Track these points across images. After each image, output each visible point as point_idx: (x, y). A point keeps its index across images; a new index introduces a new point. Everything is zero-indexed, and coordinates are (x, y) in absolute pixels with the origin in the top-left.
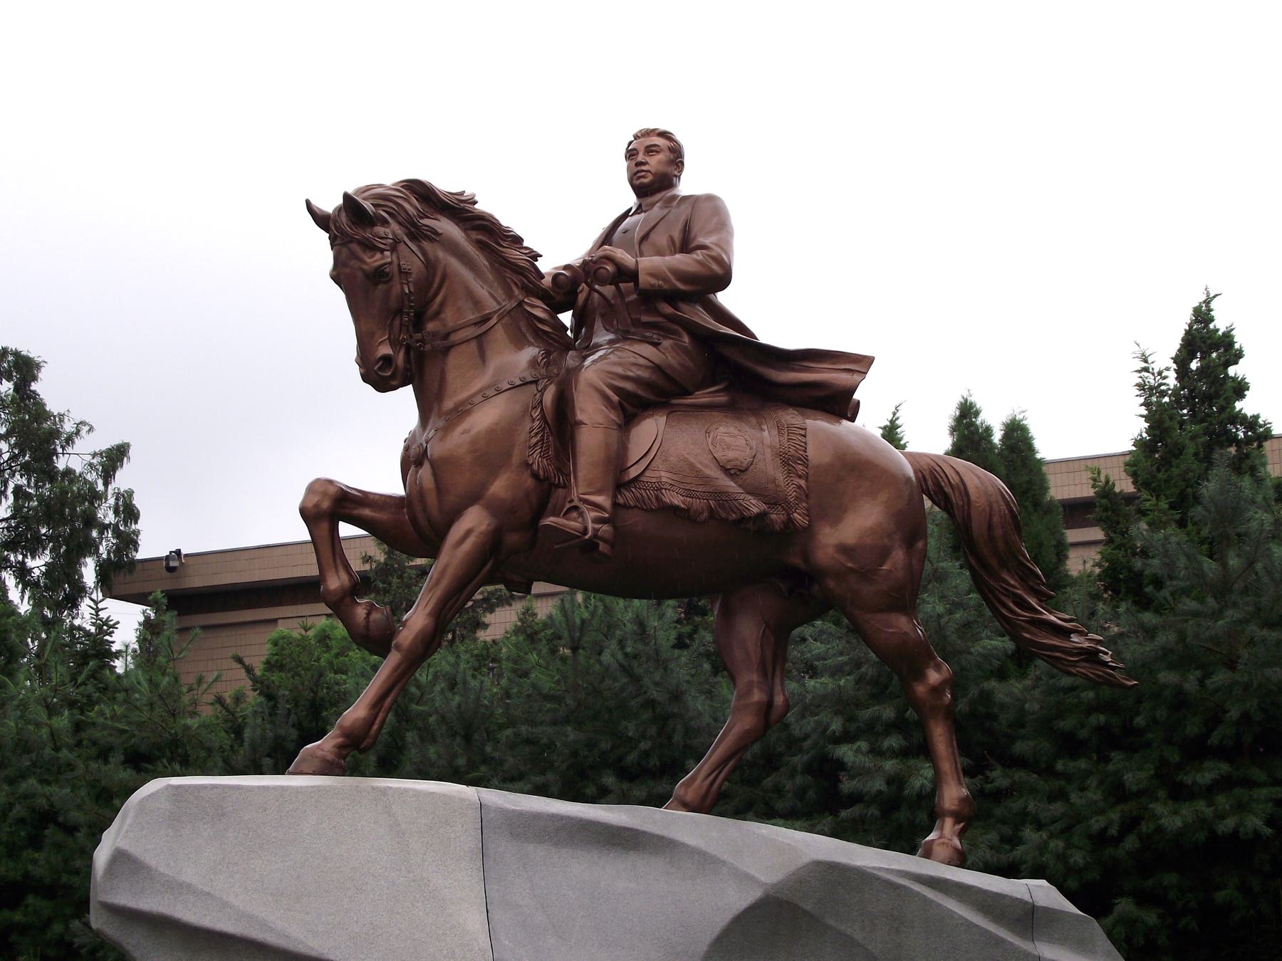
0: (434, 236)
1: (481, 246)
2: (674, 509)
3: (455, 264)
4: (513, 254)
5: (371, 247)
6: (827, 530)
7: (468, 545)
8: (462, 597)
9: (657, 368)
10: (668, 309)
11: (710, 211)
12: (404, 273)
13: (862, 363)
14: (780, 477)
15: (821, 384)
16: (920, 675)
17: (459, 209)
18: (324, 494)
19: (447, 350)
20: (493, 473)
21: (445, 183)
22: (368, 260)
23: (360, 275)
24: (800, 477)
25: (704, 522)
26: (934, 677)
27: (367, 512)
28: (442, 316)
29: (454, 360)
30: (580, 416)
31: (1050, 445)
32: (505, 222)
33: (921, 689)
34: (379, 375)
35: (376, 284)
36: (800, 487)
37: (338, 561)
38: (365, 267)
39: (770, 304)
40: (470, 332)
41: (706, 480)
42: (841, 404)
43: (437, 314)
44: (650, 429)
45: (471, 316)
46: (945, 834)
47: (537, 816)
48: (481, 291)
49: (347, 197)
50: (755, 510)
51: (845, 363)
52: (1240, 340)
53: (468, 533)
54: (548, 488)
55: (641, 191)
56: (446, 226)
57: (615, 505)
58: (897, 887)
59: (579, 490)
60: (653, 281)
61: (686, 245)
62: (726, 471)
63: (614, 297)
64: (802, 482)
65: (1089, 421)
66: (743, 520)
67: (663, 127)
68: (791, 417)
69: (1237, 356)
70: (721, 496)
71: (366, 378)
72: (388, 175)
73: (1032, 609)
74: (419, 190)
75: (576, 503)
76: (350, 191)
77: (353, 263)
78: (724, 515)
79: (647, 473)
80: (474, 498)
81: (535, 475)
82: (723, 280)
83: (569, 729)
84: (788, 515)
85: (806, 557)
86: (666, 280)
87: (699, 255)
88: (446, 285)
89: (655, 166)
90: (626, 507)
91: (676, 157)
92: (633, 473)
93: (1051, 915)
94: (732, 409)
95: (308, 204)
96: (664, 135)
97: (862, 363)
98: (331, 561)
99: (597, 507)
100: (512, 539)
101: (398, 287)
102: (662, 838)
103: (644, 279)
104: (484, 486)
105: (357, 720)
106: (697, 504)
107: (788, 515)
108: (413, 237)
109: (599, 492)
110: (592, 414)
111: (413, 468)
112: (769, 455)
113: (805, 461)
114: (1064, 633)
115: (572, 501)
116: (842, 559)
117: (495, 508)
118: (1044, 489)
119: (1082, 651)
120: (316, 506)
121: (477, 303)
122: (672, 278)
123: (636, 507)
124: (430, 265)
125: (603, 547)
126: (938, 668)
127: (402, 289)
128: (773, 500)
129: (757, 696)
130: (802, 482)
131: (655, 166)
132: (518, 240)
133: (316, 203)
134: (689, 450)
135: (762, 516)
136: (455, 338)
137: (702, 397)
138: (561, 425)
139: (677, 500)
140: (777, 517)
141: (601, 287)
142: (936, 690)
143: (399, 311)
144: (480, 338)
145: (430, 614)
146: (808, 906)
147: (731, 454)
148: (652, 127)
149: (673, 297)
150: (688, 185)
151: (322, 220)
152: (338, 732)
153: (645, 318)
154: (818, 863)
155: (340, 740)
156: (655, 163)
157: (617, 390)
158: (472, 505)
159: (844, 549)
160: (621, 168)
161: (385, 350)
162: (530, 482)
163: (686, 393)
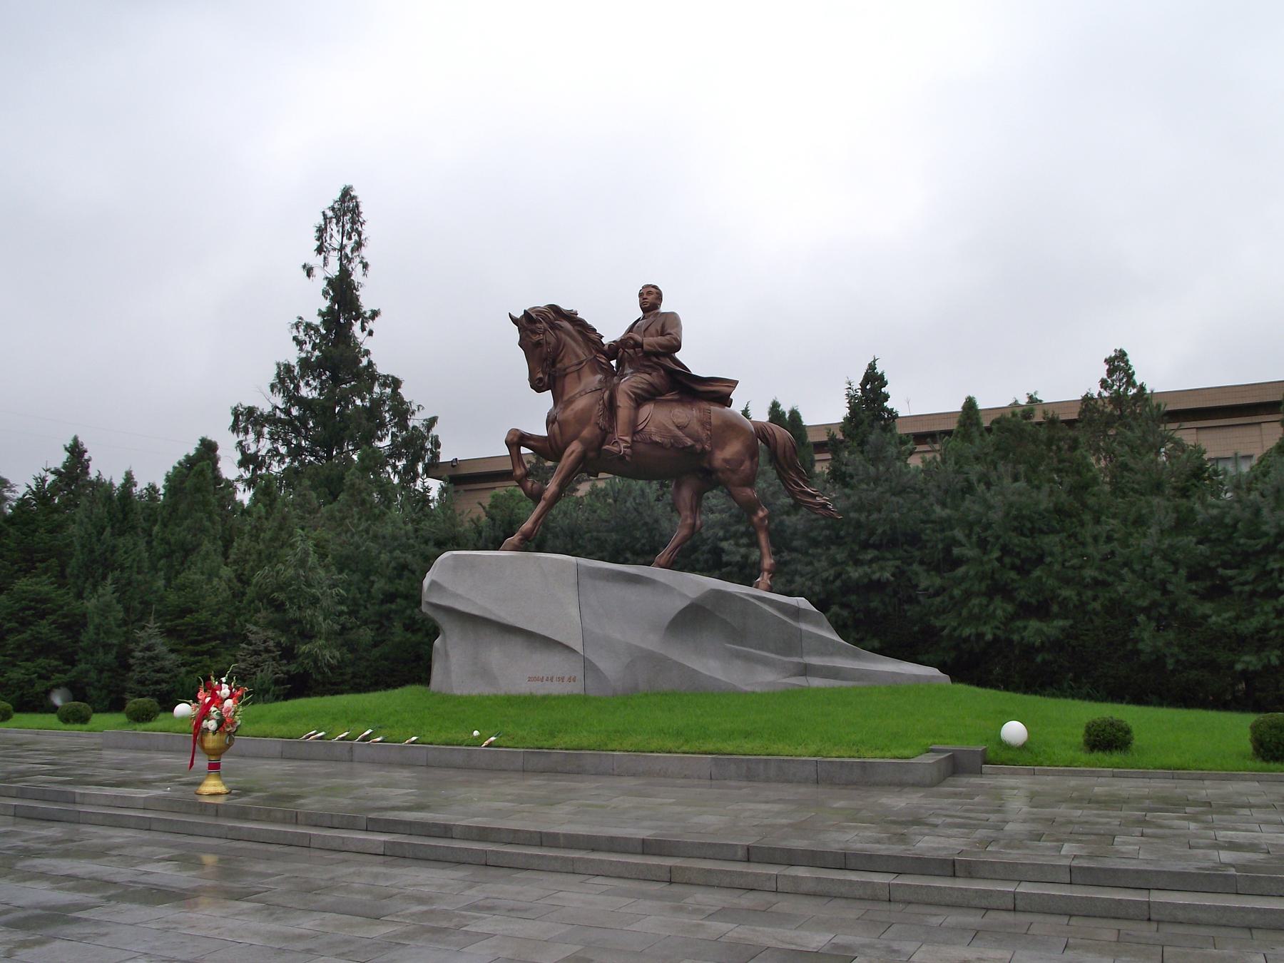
0: (561, 328)
1: (579, 332)
7: (573, 457)
9: (651, 384)
11: (673, 319)
16: (755, 513)
17: (571, 317)
21: (565, 306)
26: (761, 514)
34: (538, 386)
39: (696, 358)
42: (725, 400)
44: (647, 410)
45: (575, 362)
47: (599, 569)
48: (580, 352)
54: (605, 434)
56: (566, 324)
57: (633, 441)
66: (685, 448)
69: (885, 384)
72: (542, 303)
74: (554, 309)
82: (678, 348)
87: (668, 337)
89: (650, 298)
91: (659, 296)
93: (806, 612)
94: (680, 401)
96: (655, 287)
113: (710, 424)
117: (583, 442)
121: (577, 356)
124: (558, 340)
131: (650, 298)
135: (692, 446)
139: (658, 439)
140: (698, 447)
142: (762, 519)
143: (546, 359)
149: (657, 355)
150: (664, 308)
151: (515, 321)
156: (650, 298)
162: (598, 431)
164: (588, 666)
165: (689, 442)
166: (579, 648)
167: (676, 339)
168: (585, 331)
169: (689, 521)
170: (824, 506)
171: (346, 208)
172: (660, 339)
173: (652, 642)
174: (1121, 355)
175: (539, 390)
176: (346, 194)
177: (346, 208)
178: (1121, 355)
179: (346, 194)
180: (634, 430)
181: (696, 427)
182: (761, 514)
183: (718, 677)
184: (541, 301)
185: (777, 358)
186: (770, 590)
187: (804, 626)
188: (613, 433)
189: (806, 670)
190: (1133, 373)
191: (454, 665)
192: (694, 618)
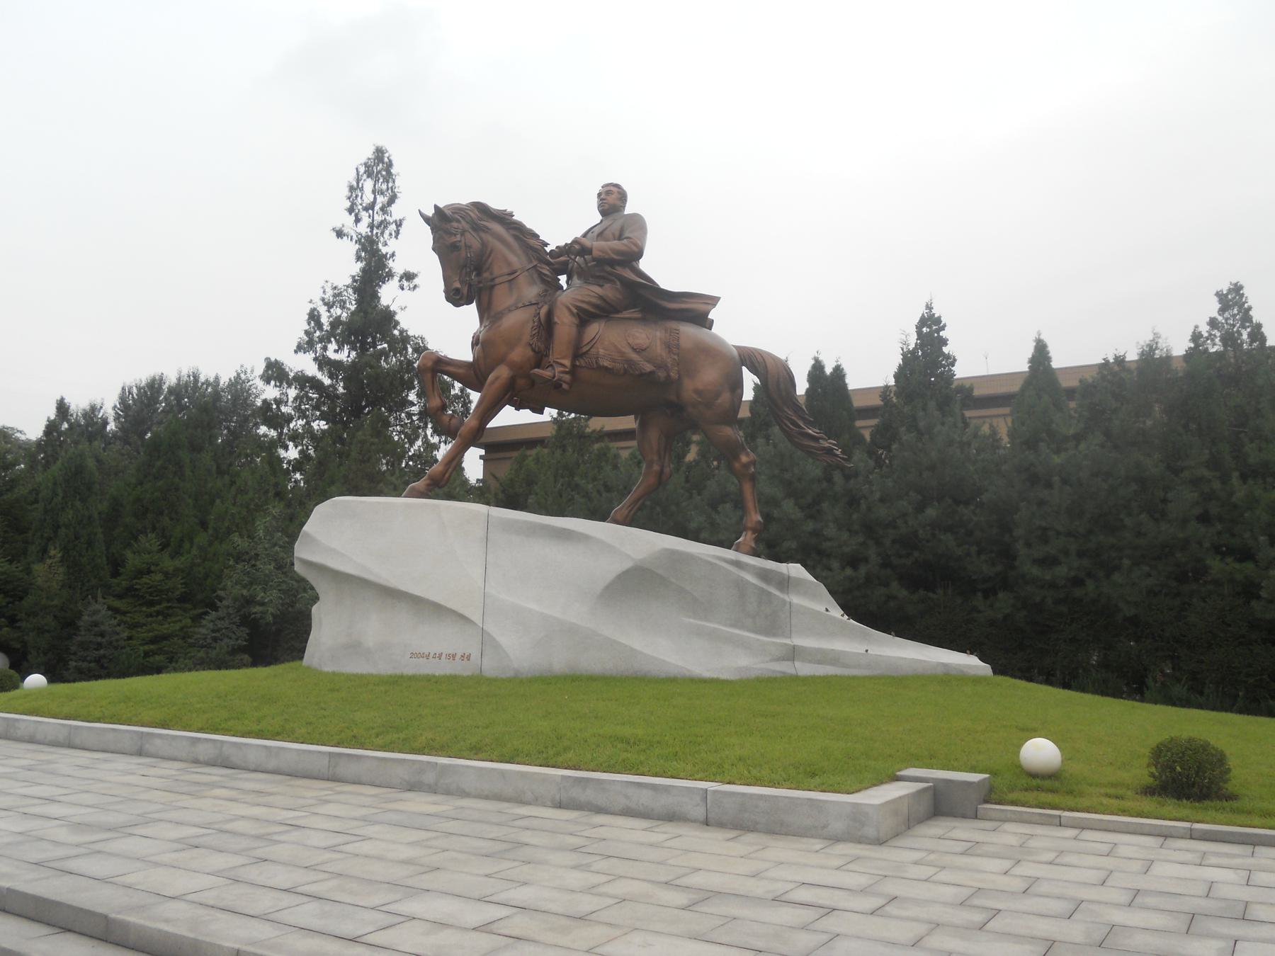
0: (486, 230)
1: (516, 237)
2: (606, 368)
3: (498, 245)
4: (532, 242)
5: (451, 234)
7: (497, 384)
9: (601, 297)
10: (609, 269)
11: (637, 222)
12: (468, 247)
13: (713, 301)
14: (664, 354)
15: (695, 309)
16: (737, 458)
17: (504, 219)
19: (492, 287)
21: (496, 204)
26: (744, 459)
31: (854, 382)
32: (528, 226)
33: (737, 465)
34: (456, 297)
39: (664, 266)
41: (622, 354)
42: (702, 320)
44: (594, 329)
45: (506, 270)
46: (746, 538)
47: (516, 521)
48: (513, 259)
52: (944, 320)
54: (540, 359)
55: (604, 213)
56: (497, 228)
57: (574, 366)
58: (711, 563)
61: (620, 238)
62: (634, 350)
65: (871, 369)
66: (642, 375)
68: (673, 325)
69: (943, 328)
70: (630, 362)
71: (448, 299)
72: (464, 199)
73: (799, 427)
74: (481, 208)
76: (441, 206)
81: (534, 350)
82: (639, 255)
87: (625, 241)
89: (611, 201)
90: (580, 367)
91: (623, 197)
92: (585, 349)
93: (799, 582)
94: (644, 320)
96: (617, 186)
97: (713, 301)
100: (521, 382)
102: (582, 534)
103: (595, 253)
106: (618, 366)
108: (474, 230)
109: (563, 358)
110: (565, 324)
112: (658, 343)
113: (678, 346)
114: (816, 439)
116: (695, 396)
117: (512, 366)
118: (850, 403)
119: (824, 449)
121: (509, 264)
124: (484, 244)
125: (565, 386)
126: (748, 455)
128: (662, 366)
131: (611, 201)
132: (536, 236)
134: (619, 340)
135: (652, 373)
136: (497, 281)
137: (626, 314)
138: (547, 327)
139: (606, 364)
140: (661, 374)
141: (574, 257)
142: (746, 466)
143: (465, 266)
146: (660, 572)
147: (638, 341)
149: (612, 263)
150: (628, 210)
151: (427, 220)
154: (667, 550)
156: (612, 199)
157: (577, 307)
159: (698, 392)
160: (594, 202)
161: (458, 285)
162: (530, 353)
163: (618, 312)
164: (485, 638)
165: (648, 368)
166: (476, 618)
167: (636, 245)
168: (524, 237)
169: (656, 468)
170: (829, 451)
171: (379, 166)
172: (615, 244)
173: (577, 614)
174: (1237, 289)
175: (457, 303)
176: (380, 153)
177: (379, 166)
178: (1237, 289)
179: (380, 153)
180: (578, 353)
181: (659, 350)
182: (744, 459)
183: (667, 659)
184: (461, 195)
185: (802, 287)
186: (756, 554)
187: (796, 600)
188: (547, 356)
189: (793, 654)
190: (1250, 308)
191: (333, 636)
192: (636, 584)
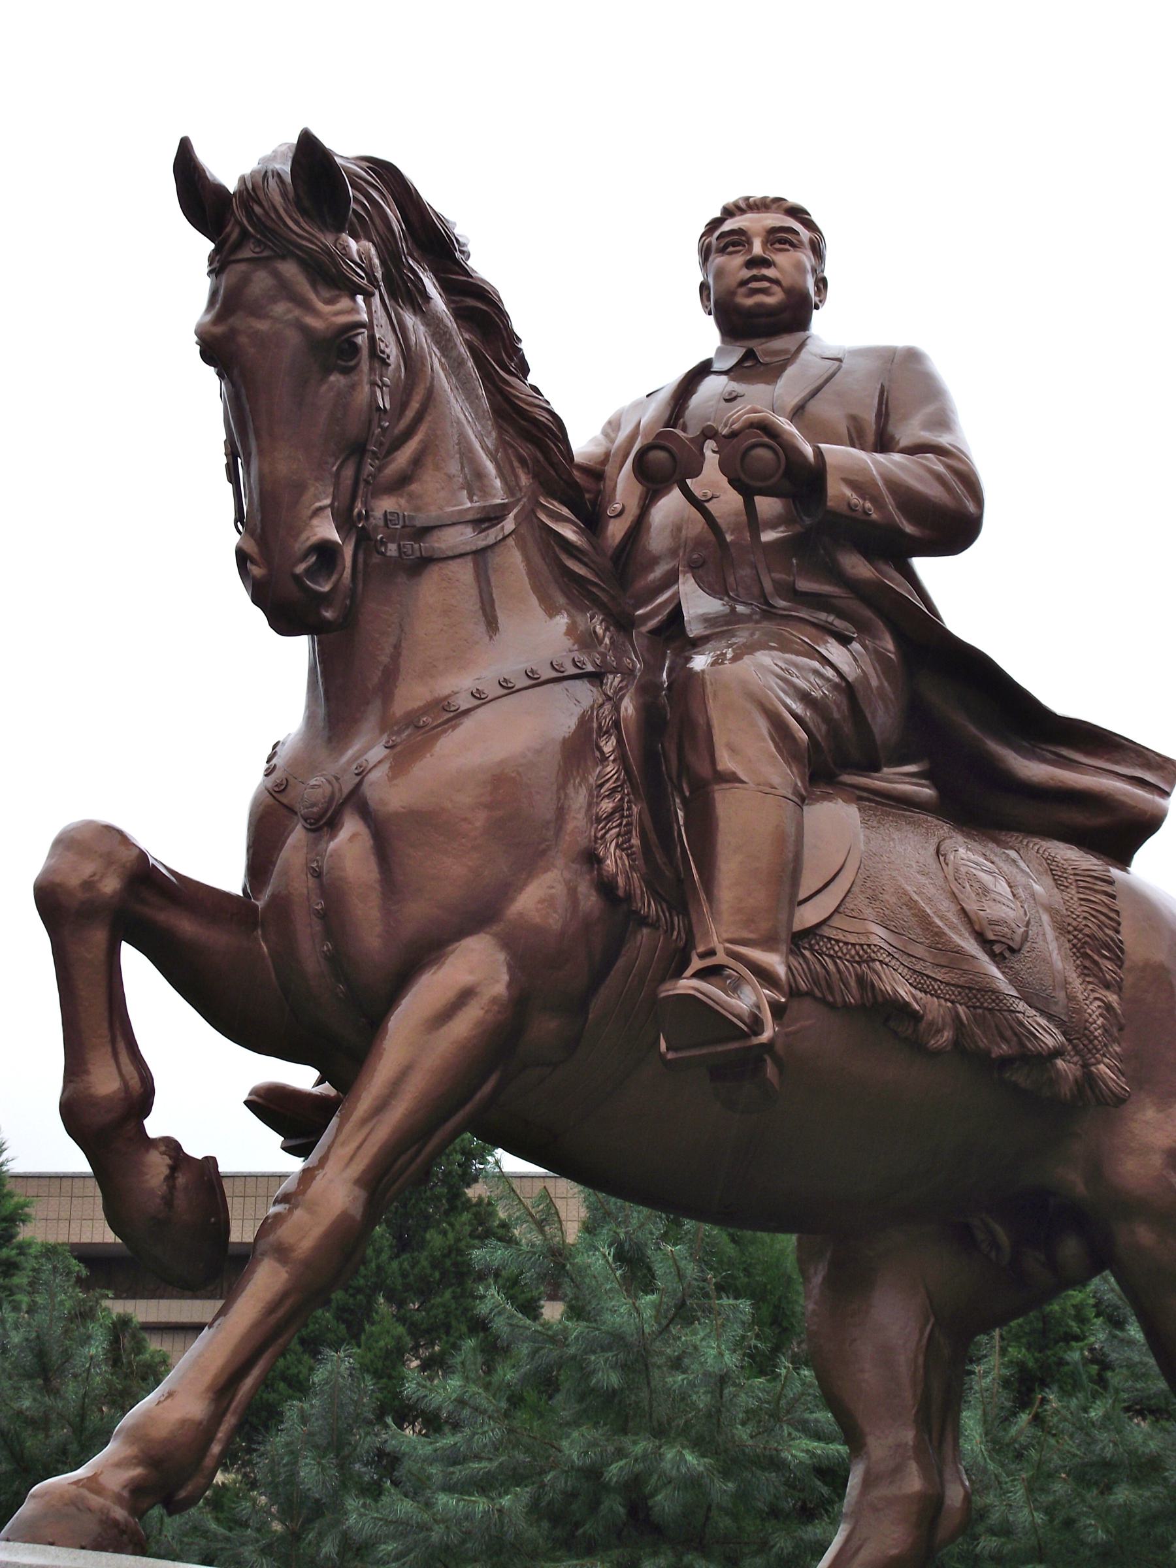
6: (1150, 1114)
7: (463, 1025)
8: (429, 1148)
11: (898, 395)
18: (109, 860)
19: (425, 562)
20: (530, 859)
22: (320, 306)
23: (293, 338)
24: (1107, 986)
25: (937, 1053)
27: (187, 926)
28: (414, 487)
29: (430, 590)
30: (726, 762)
35: (327, 371)
36: (1108, 1007)
37: (119, 1038)
38: (310, 321)
40: (462, 537)
43: (402, 482)
49: (309, 149)
50: (1050, 1042)
51: (1134, 765)
53: (465, 996)
59: (718, 934)
60: (854, 498)
62: (985, 943)
63: (735, 529)
64: (1113, 998)
67: (793, 199)
75: (721, 958)
77: (280, 308)
78: (983, 1042)
79: (837, 921)
80: (479, 914)
83: (383, 1547)
84: (1085, 1066)
85: (1096, 1171)
86: (877, 500)
88: (428, 418)
95: (185, 151)
98: (104, 1029)
99: (765, 976)
101: (367, 388)
103: (837, 491)
104: (506, 890)
105: (183, 1422)
106: (933, 1007)
107: (1085, 1066)
111: (297, 835)
113: (1117, 953)
115: (712, 953)
120: (88, 885)
122: (889, 500)
123: (809, 994)
127: (373, 394)
129: (914, 1482)
130: (1113, 998)
133: (204, 155)
144: (479, 555)
145: (359, 1182)
148: (772, 194)
152: (130, 1451)
153: (804, 585)
155: (137, 1472)
158: (471, 933)
162: (590, 900)
